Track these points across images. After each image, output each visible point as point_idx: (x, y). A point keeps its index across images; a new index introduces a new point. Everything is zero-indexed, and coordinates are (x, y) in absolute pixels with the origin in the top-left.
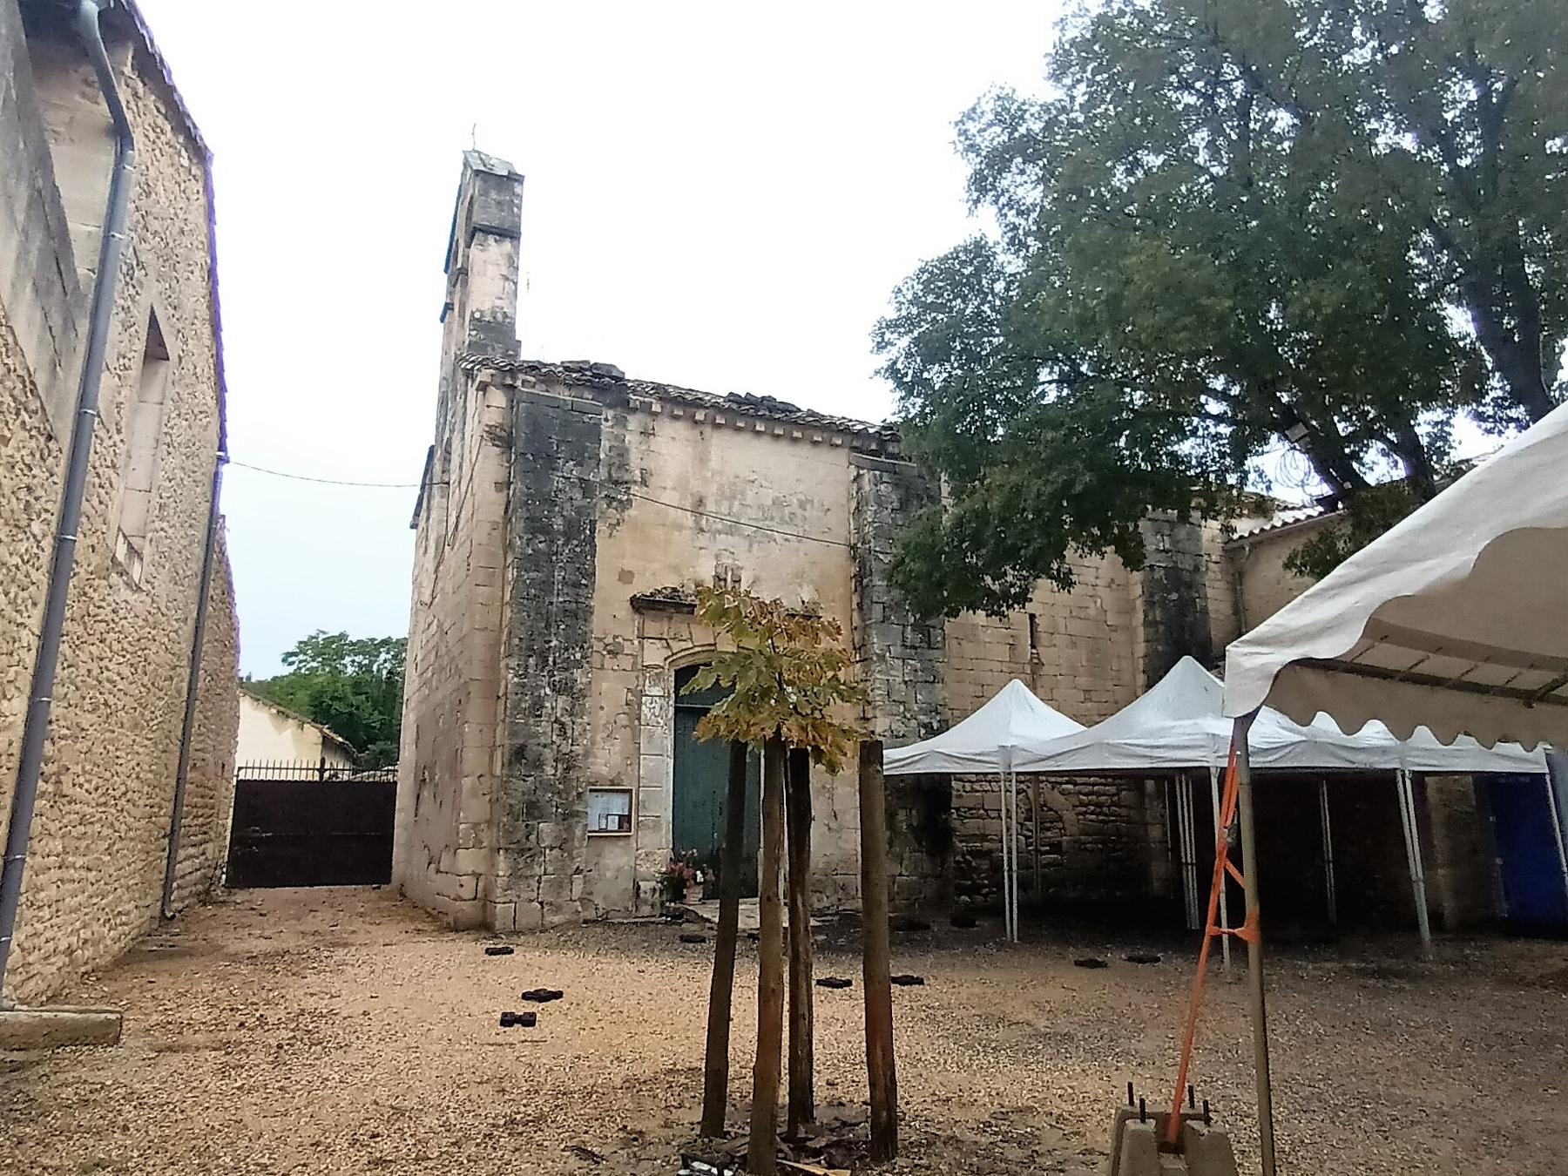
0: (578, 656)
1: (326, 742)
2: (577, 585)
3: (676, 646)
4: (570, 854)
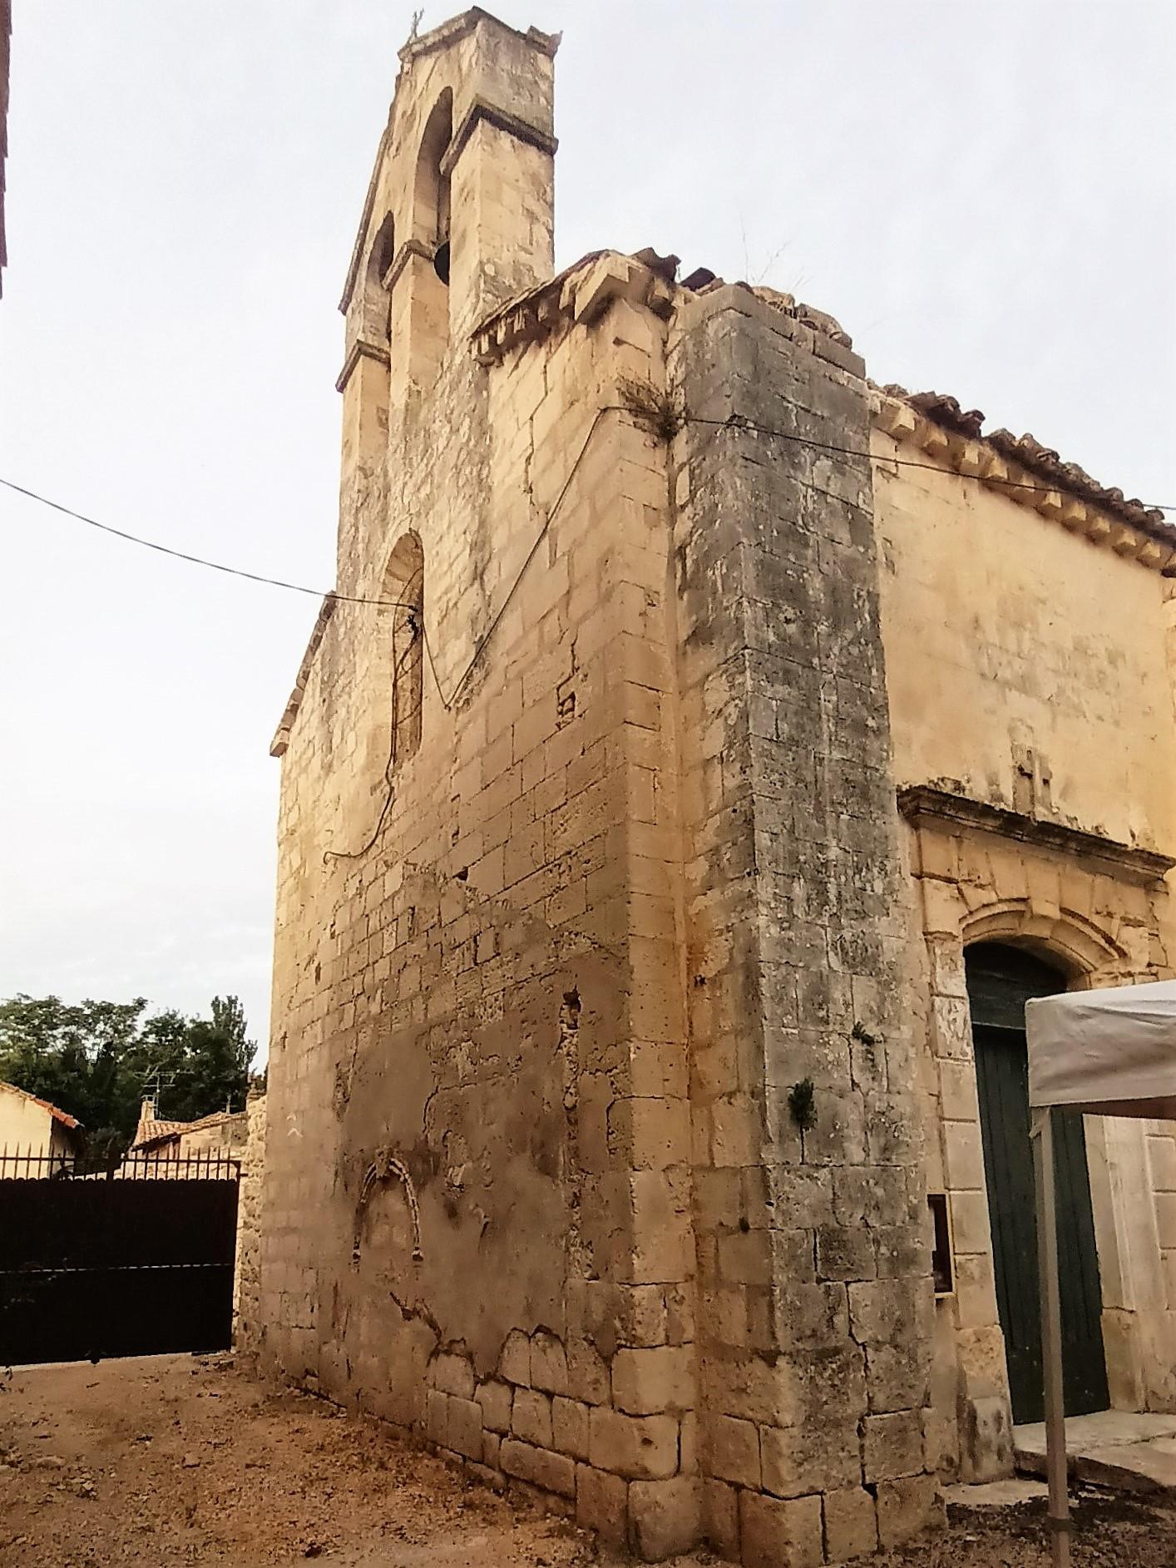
0: (879, 886)
1: (57, 1126)
2: (861, 728)
3: (976, 897)
4: (913, 1359)
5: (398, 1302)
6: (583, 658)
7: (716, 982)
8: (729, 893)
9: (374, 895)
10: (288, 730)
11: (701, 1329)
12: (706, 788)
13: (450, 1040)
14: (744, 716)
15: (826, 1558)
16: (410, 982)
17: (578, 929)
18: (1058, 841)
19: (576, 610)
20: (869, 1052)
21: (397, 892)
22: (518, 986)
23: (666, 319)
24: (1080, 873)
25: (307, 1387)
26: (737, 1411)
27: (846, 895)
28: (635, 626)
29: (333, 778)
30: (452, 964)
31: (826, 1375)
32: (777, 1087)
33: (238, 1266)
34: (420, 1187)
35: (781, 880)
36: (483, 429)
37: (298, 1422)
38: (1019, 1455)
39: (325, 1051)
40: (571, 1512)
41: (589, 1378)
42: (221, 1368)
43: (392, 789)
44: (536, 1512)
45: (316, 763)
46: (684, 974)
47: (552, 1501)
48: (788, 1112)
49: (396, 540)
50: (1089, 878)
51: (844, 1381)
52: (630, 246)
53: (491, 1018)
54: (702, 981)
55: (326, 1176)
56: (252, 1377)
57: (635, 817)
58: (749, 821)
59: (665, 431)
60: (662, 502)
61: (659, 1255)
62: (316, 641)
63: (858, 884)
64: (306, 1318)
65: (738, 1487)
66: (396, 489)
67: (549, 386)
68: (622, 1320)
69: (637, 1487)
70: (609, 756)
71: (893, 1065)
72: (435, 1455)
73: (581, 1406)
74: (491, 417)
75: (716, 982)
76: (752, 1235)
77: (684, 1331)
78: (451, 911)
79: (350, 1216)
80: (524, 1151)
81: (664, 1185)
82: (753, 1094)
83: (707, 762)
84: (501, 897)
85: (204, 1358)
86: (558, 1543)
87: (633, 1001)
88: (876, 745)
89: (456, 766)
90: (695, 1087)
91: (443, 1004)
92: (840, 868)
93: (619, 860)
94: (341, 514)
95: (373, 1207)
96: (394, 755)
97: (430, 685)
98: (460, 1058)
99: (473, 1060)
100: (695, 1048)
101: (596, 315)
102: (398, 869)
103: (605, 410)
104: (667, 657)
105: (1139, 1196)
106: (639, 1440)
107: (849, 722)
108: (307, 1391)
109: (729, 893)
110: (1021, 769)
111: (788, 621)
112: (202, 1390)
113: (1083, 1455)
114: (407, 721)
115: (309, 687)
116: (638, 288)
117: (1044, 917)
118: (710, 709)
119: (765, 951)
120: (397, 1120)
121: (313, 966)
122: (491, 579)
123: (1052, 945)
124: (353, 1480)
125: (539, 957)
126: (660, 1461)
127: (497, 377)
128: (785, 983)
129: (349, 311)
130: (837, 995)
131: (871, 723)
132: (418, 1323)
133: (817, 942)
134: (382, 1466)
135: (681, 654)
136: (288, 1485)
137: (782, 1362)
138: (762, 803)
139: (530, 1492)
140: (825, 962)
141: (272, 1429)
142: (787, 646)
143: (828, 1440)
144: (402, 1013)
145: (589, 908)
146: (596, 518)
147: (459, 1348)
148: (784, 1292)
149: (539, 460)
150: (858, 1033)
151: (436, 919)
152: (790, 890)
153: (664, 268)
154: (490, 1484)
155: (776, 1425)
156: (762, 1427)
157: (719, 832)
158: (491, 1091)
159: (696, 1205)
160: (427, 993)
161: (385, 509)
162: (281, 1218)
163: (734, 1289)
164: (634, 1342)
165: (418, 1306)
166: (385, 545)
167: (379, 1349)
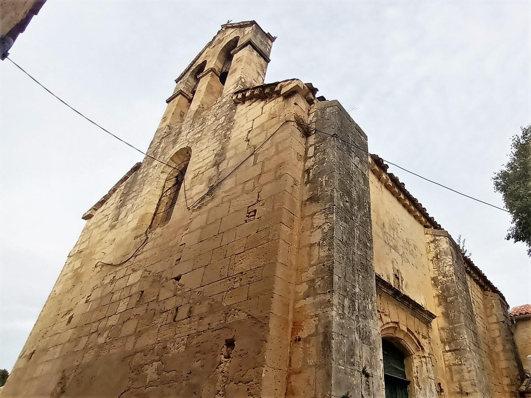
2: (365, 245)
3: (386, 319)
6: (263, 197)
7: (306, 341)
12: (310, 255)
14: (332, 229)
17: (239, 308)
18: (407, 303)
19: (262, 180)
22: (199, 334)
23: (310, 104)
24: (411, 316)
27: (361, 308)
28: (289, 190)
29: (114, 231)
30: (159, 320)
35: (341, 297)
36: (230, 120)
45: (107, 224)
49: (179, 149)
52: (305, 80)
53: (176, 349)
54: (300, 339)
57: (280, 261)
59: (306, 133)
60: (303, 154)
62: (125, 178)
63: (364, 305)
66: (184, 133)
67: (263, 112)
70: (271, 235)
71: (375, 388)
74: (235, 118)
75: (306, 341)
78: (165, 294)
83: (311, 245)
84: (199, 290)
87: (269, 345)
89: (186, 232)
91: (147, 341)
93: (270, 279)
94: (154, 138)
96: (150, 227)
97: (181, 199)
98: (150, 372)
99: (159, 372)
100: (291, 373)
101: (288, 96)
102: (139, 273)
103: (287, 121)
104: (298, 204)
110: (396, 275)
111: (347, 202)
115: (114, 195)
116: (305, 93)
117: (403, 331)
118: (315, 225)
119: (335, 328)
121: (68, 317)
122: (223, 166)
123: (402, 342)
125: (215, 320)
127: (240, 107)
128: (341, 343)
129: (179, 82)
130: (357, 352)
131: (368, 244)
133: (351, 327)
135: (304, 204)
138: (336, 264)
142: (346, 210)
144: (119, 343)
145: (249, 298)
146: (278, 152)
149: (254, 133)
150: (364, 372)
153: (314, 91)
157: (316, 273)
160: (138, 334)
161: (177, 139)
166: (173, 150)
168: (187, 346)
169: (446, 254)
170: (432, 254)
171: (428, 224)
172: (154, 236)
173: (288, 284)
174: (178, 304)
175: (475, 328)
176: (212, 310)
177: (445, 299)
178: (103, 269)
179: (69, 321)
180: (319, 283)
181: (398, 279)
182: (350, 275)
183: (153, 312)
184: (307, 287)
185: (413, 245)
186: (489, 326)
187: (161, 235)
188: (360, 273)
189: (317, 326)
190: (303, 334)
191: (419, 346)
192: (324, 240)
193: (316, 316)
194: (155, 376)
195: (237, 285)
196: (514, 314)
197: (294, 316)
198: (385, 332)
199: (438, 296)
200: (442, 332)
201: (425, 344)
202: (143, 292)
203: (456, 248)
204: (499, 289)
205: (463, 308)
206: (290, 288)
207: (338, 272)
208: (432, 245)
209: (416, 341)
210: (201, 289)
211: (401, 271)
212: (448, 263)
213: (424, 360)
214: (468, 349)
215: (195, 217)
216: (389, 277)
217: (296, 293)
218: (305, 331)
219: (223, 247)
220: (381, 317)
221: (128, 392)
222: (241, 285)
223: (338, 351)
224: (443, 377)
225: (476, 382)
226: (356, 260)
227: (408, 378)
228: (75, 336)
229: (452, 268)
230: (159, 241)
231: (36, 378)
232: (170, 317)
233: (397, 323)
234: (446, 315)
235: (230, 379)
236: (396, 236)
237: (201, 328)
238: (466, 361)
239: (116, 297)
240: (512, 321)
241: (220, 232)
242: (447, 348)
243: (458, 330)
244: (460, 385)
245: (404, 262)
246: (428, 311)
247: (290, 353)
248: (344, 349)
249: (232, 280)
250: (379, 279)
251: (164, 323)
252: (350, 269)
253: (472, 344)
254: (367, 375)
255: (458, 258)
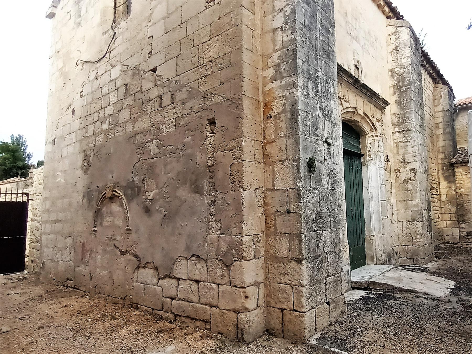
3: (346, 105)
5: (118, 248)
8: (284, 82)
9: (105, 79)
10: (56, 7)
11: (267, 251)
12: (274, 40)
13: (146, 139)
14: (293, 12)
15: (316, 331)
16: (125, 115)
20: (329, 148)
21: (117, 78)
22: (184, 116)
24: (368, 103)
25: (67, 285)
26: (283, 281)
27: (324, 91)
31: (316, 265)
32: (304, 157)
33: (28, 237)
34: (130, 200)
37: (65, 302)
38: (353, 282)
39: (78, 145)
40: (208, 327)
41: (219, 274)
42: (21, 280)
43: (115, 33)
44: (191, 328)
46: (262, 114)
47: (198, 323)
48: (306, 168)
50: (370, 104)
51: (321, 266)
53: (169, 129)
55: (78, 198)
56: (37, 283)
58: (295, 54)
61: (252, 223)
63: (327, 88)
64: (66, 256)
65: (283, 310)
68: (236, 250)
69: (242, 315)
70: (233, 20)
72: (137, 309)
73: (214, 286)
76: (292, 214)
77: (260, 253)
78: (146, 85)
79: (91, 214)
80: (186, 184)
81: (254, 196)
82: (294, 161)
83: (274, 31)
85: (10, 276)
86: (206, 342)
87: (244, 121)
88: (332, 38)
89: (150, 24)
90: (266, 159)
91: (143, 124)
92: (322, 80)
93: (239, 64)
95: (104, 210)
96: (114, 21)
98: (153, 147)
100: (266, 143)
105: (377, 202)
106: (243, 297)
107: (324, 27)
108: (67, 287)
109: (284, 82)
110: (356, 66)
112: (10, 292)
113: (370, 280)
114: (121, 7)
117: (360, 115)
119: (300, 106)
120: (116, 173)
121: (70, 110)
124: (99, 327)
125: (196, 104)
126: (251, 304)
130: (321, 126)
131: (331, 30)
132: (128, 256)
133: (315, 106)
134: (113, 318)
136: (64, 334)
137: (304, 262)
138: (299, 48)
139: (187, 320)
140: (317, 113)
141: (52, 307)
143: (317, 288)
144: (120, 129)
147: (149, 265)
148: (305, 236)
150: (326, 142)
151: (139, 89)
152: (307, 84)
154: (167, 319)
155: (302, 285)
156: (294, 287)
157: (280, 57)
158: (169, 160)
159: (265, 204)
160: (134, 120)
162: (53, 217)
163: (283, 235)
164: (242, 258)
165: (129, 249)
167: (104, 267)
168: (176, 126)
169: (405, 46)
170: (393, 46)
171: (391, 14)
172: (120, 31)
173: (255, 69)
174: (161, 93)
175: (423, 114)
176: (191, 96)
177: (399, 88)
178: (85, 66)
179: (73, 114)
180: (284, 67)
181: (358, 69)
182: (312, 60)
183: (141, 101)
184: (274, 71)
185: (374, 37)
186: (435, 111)
187: (127, 29)
188: (322, 58)
189: (284, 105)
190: (273, 113)
191: (374, 128)
192: (287, 23)
193: (283, 96)
194: (157, 151)
195: (209, 72)
196: (458, 104)
197: (264, 98)
198: (344, 116)
199: (394, 86)
200: (394, 117)
201: (378, 126)
202: (127, 85)
203: (416, 39)
204: (450, 82)
205: (415, 96)
206: (258, 73)
207: (301, 55)
208: (393, 37)
209: (370, 124)
210: (177, 78)
211: (361, 61)
212: (407, 52)
213: (376, 138)
214: (414, 130)
215: (155, 7)
216: (350, 67)
217: (265, 77)
218: (275, 110)
219: (189, 37)
220: (341, 103)
221: (139, 163)
222: (212, 72)
223: (304, 124)
224: (391, 151)
225: (417, 154)
226: (319, 45)
227: (362, 151)
228: (83, 125)
229: (409, 60)
230: (127, 35)
231: (65, 157)
232: (157, 105)
233: (355, 108)
234: (399, 103)
235: (217, 148)
236: (358, 27)
237: (186, 112)
238: (411, 139)
239: (105, 90)
240: (456, 110)
241: (183, 21)
242: (397, 130)
243: (407, 115)
244: (404, 157)
245: (364, 53)
246: (383, 99)
247: (264, 128)
248: (309, 123)
249: (204, 68)
250: (340, 68)
251: (153, 110)
252: (313, 53)
253: (418, 126)
254: (329, 144)
255: (417, 49)
